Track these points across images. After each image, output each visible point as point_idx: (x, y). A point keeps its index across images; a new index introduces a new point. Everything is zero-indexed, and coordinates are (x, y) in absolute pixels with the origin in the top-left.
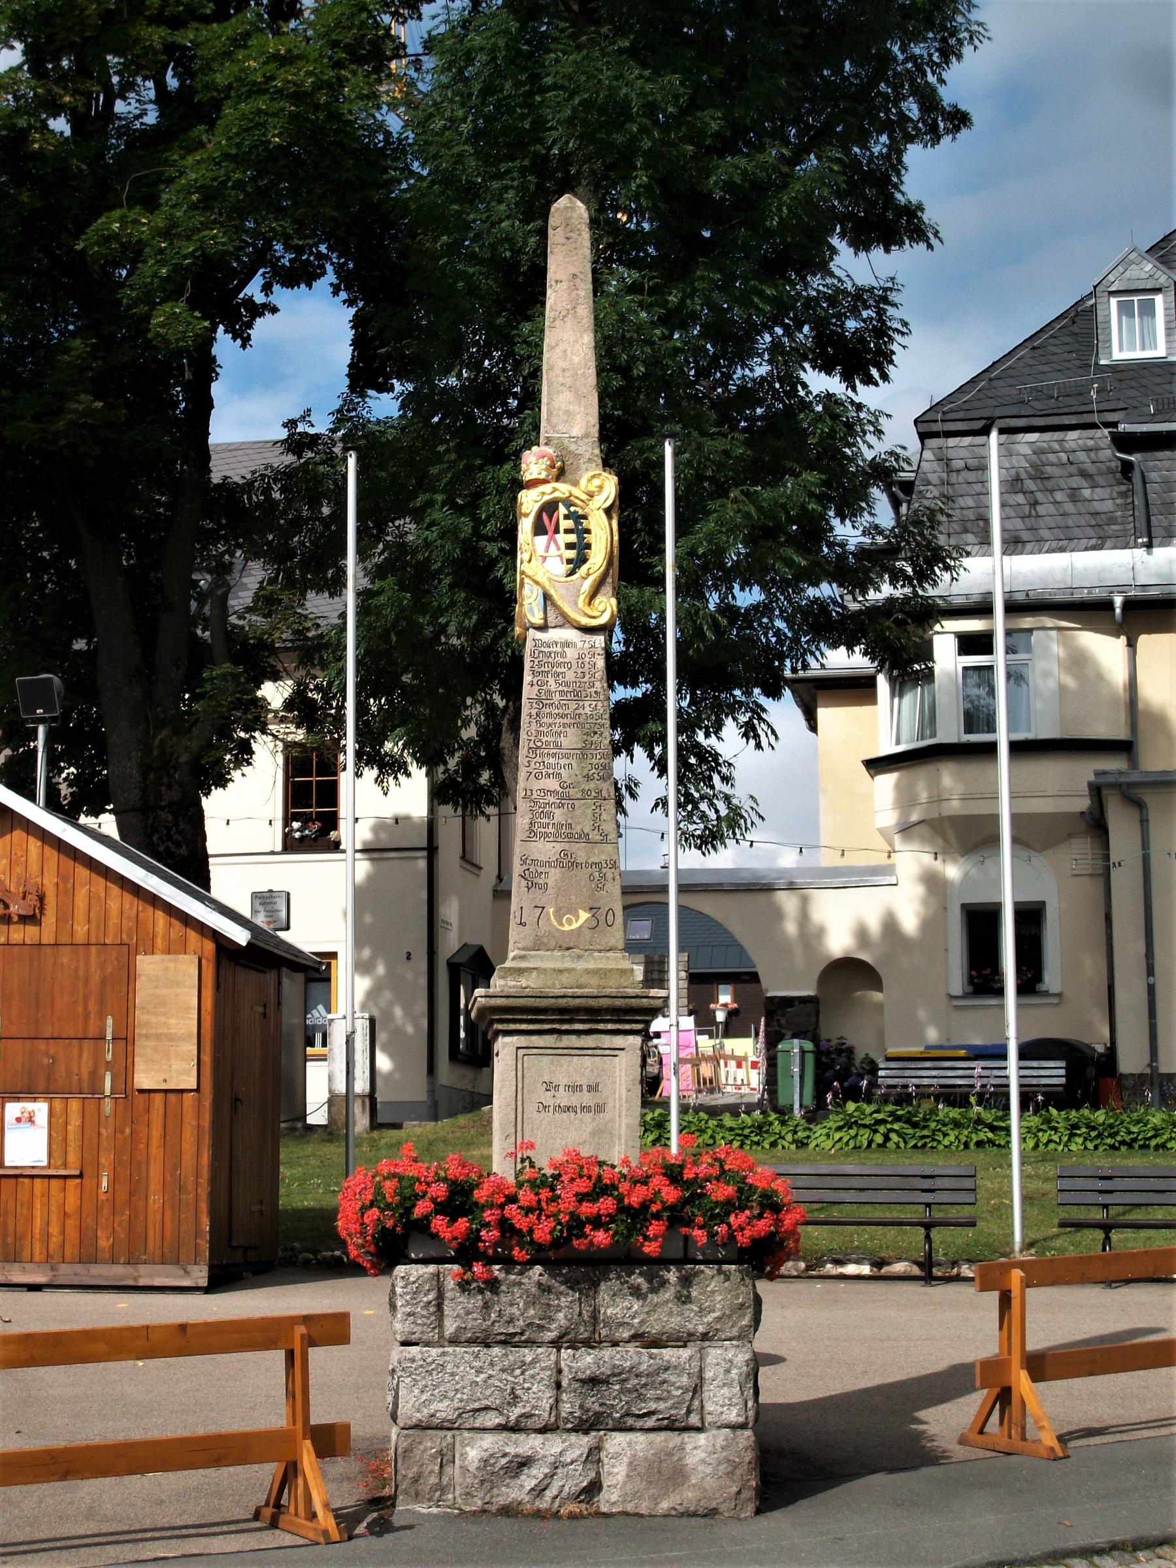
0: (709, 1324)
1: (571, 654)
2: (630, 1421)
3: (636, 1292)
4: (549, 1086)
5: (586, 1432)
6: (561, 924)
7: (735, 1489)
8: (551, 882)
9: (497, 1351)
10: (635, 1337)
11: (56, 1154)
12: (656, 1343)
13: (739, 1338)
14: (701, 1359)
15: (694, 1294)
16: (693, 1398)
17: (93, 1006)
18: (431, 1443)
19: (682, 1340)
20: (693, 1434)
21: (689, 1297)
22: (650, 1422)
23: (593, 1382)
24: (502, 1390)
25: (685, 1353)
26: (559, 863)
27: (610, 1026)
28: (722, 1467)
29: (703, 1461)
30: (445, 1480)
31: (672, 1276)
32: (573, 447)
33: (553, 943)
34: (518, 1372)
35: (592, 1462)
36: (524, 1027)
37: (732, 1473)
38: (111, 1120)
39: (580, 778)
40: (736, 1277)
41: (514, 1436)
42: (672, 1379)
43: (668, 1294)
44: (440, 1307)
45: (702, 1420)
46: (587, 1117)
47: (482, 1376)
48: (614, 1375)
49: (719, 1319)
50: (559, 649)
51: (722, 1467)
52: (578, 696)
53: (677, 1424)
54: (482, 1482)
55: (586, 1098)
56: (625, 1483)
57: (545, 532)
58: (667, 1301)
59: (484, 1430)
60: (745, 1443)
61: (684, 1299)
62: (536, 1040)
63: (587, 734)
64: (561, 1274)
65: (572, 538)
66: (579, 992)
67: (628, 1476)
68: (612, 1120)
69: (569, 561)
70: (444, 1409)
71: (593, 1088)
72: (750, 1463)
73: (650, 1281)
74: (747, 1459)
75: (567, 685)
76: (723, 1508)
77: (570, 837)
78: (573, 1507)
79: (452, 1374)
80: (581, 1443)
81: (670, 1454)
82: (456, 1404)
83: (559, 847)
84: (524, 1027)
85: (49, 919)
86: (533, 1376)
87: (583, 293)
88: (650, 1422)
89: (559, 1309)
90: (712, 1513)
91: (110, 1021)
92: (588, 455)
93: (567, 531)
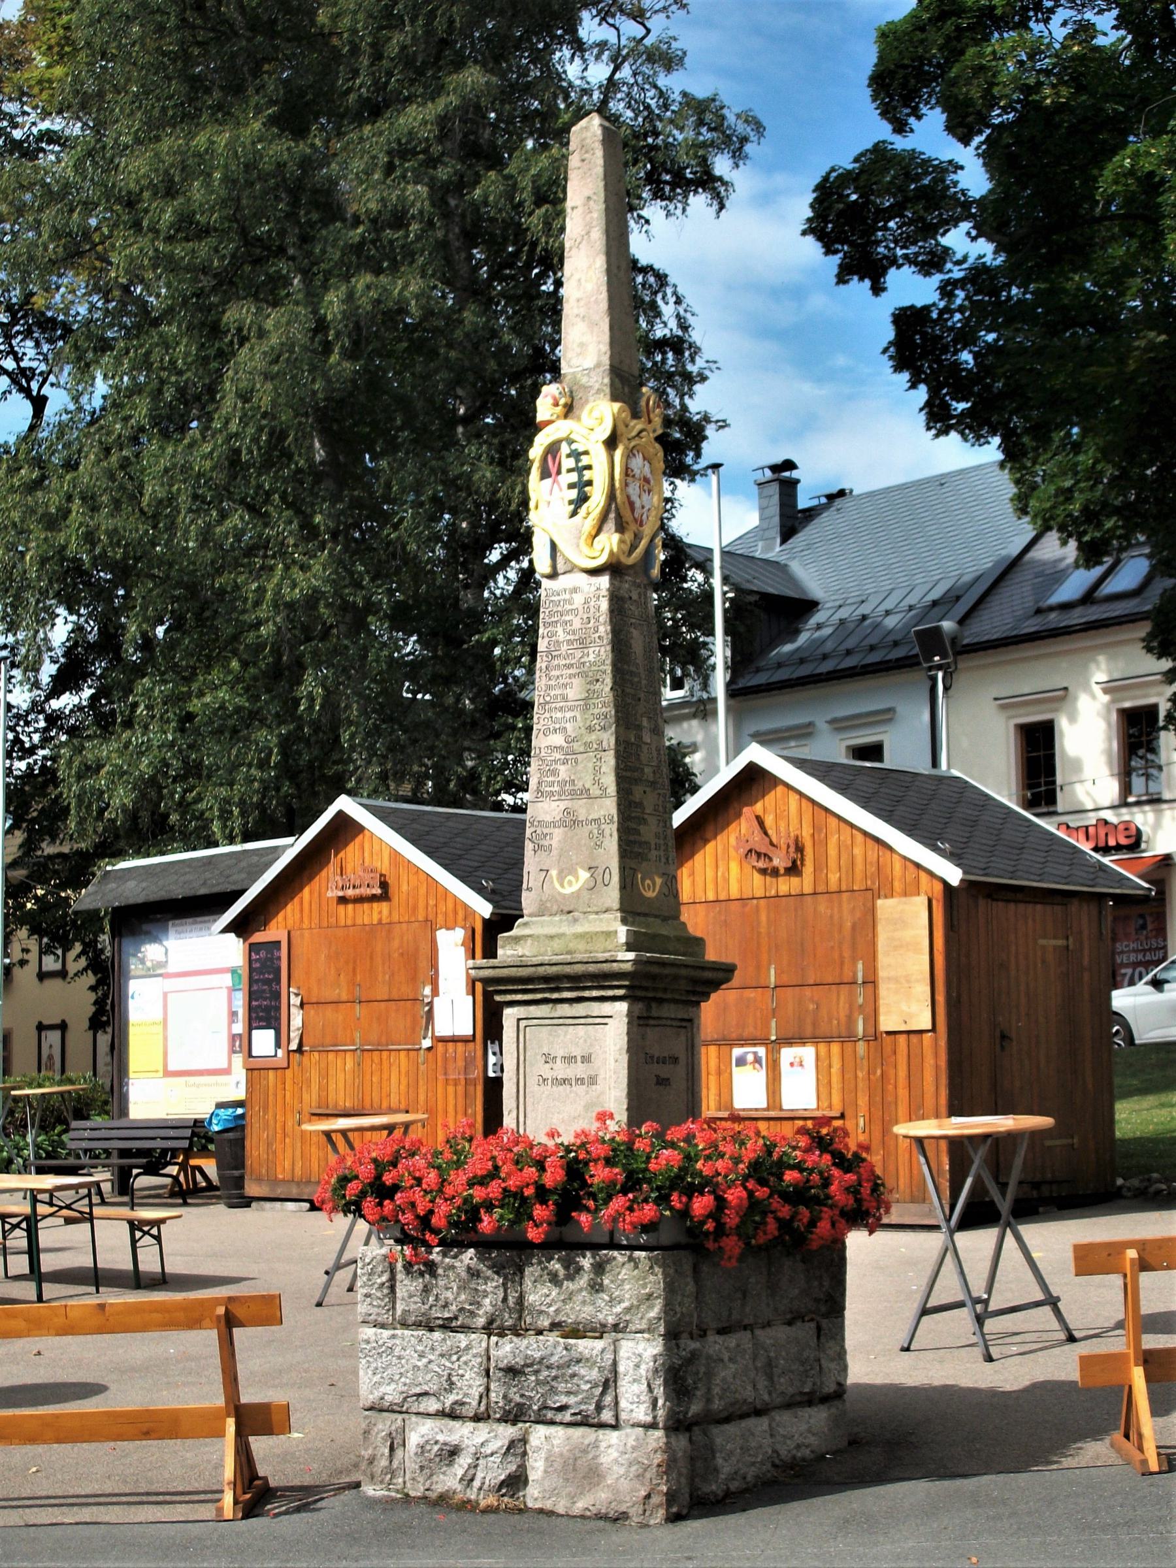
0: (618, 1315)
1: (578, 600)
2: (550, 1415)
3: (554, 1279)
4: (549, 1059)
5: (514, 1422)
6: (562, 886)
7: (643, 1493)
8: (555, 843)
9: (437, 1335)
10: (555, 1326)
11: (824, 1096)
12: (576, 1332)
13: (649, 1330)
14: (615, 1352)
15: (606, 1282)
16: (603, 1393)
17: (847, 954)
18: (385, 1424)
19: (599, 1331)
20: (608, 1432)
21: (601, 1285)
22: (567, 1417)
23: (512, 1372)
24: (440, 1376)
25: (599, 1344)
26: (562, 823)
27: (595, 993)
28: (633, 1469)
29: (616, 1461)
30: (395, 1464)
31: (586, 1262)
32: (584, 380)
33: (555, 908)
34: (454, 1358)
35: (515, 1455)
36: (519, 997)
37: (643, 1475)
38: (865, 1062)
39: (583, 731)
40: (645, 1265)
41: (452, 1423)
42: (583, 1372)
43: (583, 1281)
44: (392, 1289)
45: (617, 1417)
46: (581, 1089)
47: (425, 1360)
48: (528, 1366)
49: (628, 1310)
50: (567, 596)
51: (633, 1469)
52: (583, 643)
53: (591, 1421)
54: (422, 1468)
55: (579, 1070)
56: (543, 1478)
57: (549, 476)
58: (581, 1290)
59: (428, 1415)
60: (654, 1445)
61: (596, 1287)
62: (534, 1010)
63: (590, 683)
64: (490, 1258)
65: (574, 477)
66: (568, 958)
67: (546, 1471)
68: (603, 1093)
69: (571, 502)
70: (391, 1393)
71: (586, 1059)
72: (659, 1466)
73: (566, 1268)
74: (656, 1462)
75: (574, 633)
76: (632, 1512)
77: (573, 793)
78: (492, 1500)
79: (399, 1358)
80: (508, 1432)
81: (585, 1451)
82: (401, 1388)
83: (563, 805)
84: (519, 997)
85: (808, 870)
86: (466, 1363)
87: (595, 215)
88: (567, 1417)
89: (485, 1294)
90: (623, 1516)
91: (860, 966)
92: (597, 386)
93: (569, 471)
